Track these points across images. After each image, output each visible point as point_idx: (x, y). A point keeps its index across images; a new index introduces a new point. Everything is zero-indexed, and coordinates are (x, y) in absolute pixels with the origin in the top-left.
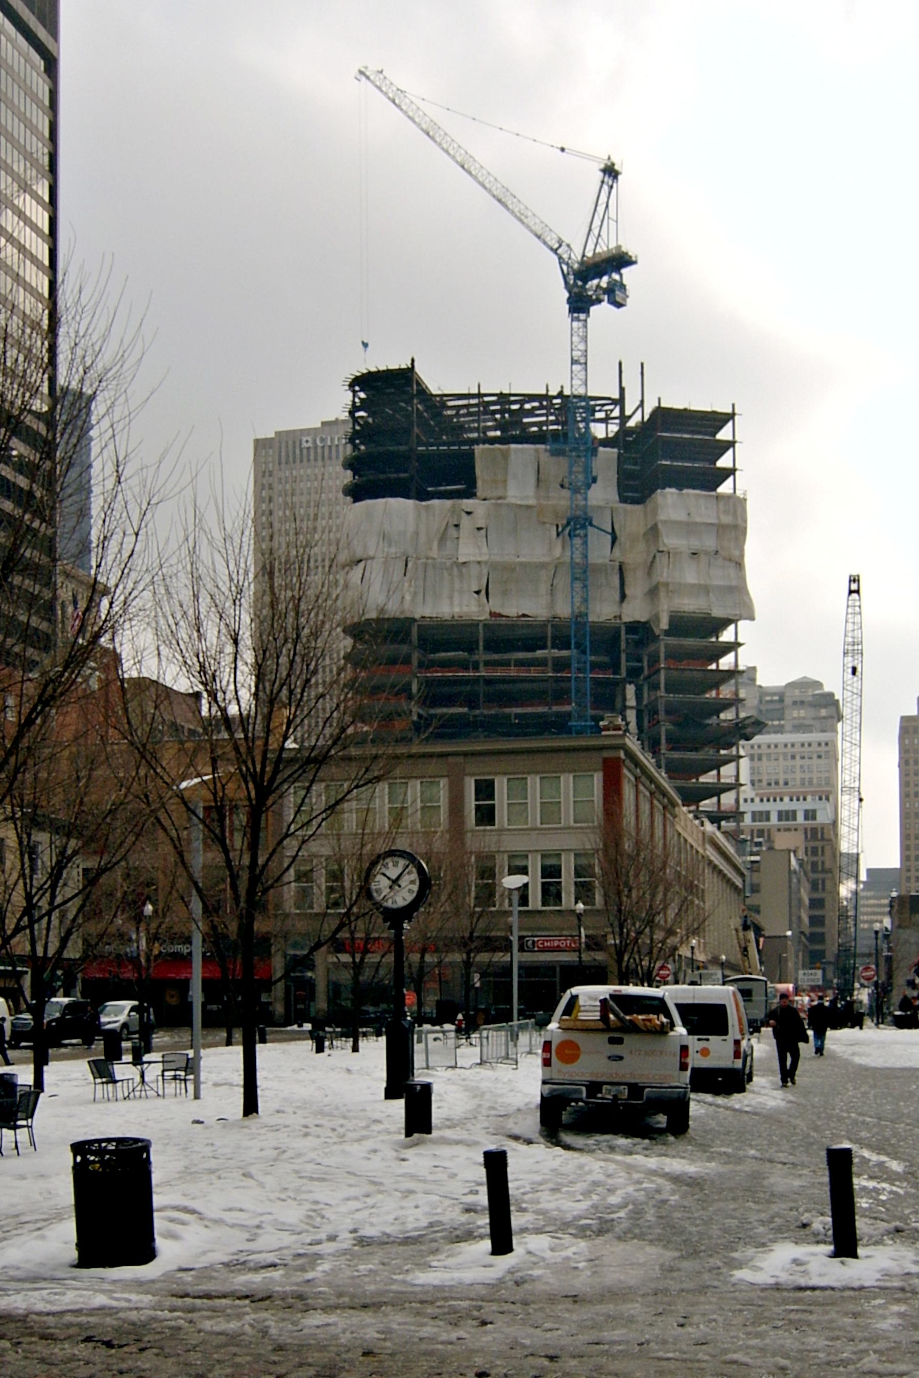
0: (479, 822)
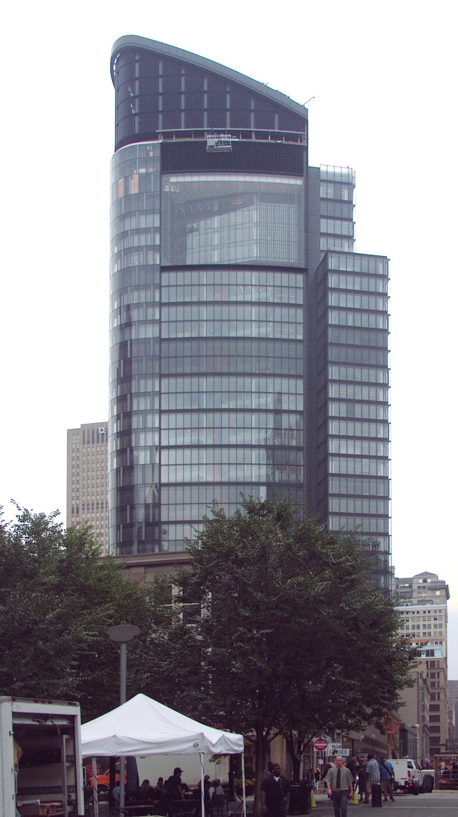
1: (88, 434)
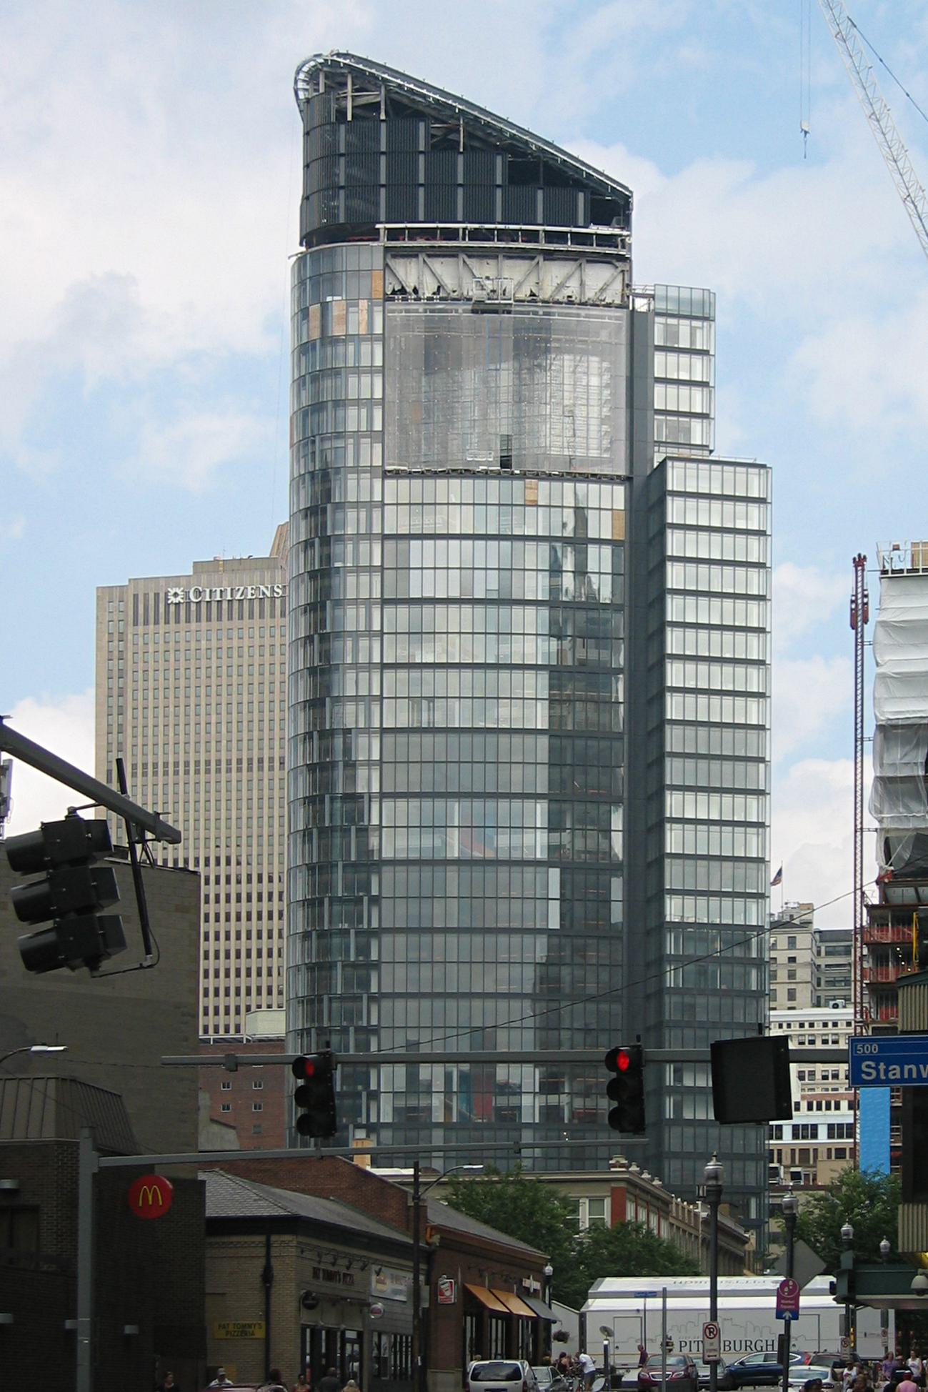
0: (792, 1173)
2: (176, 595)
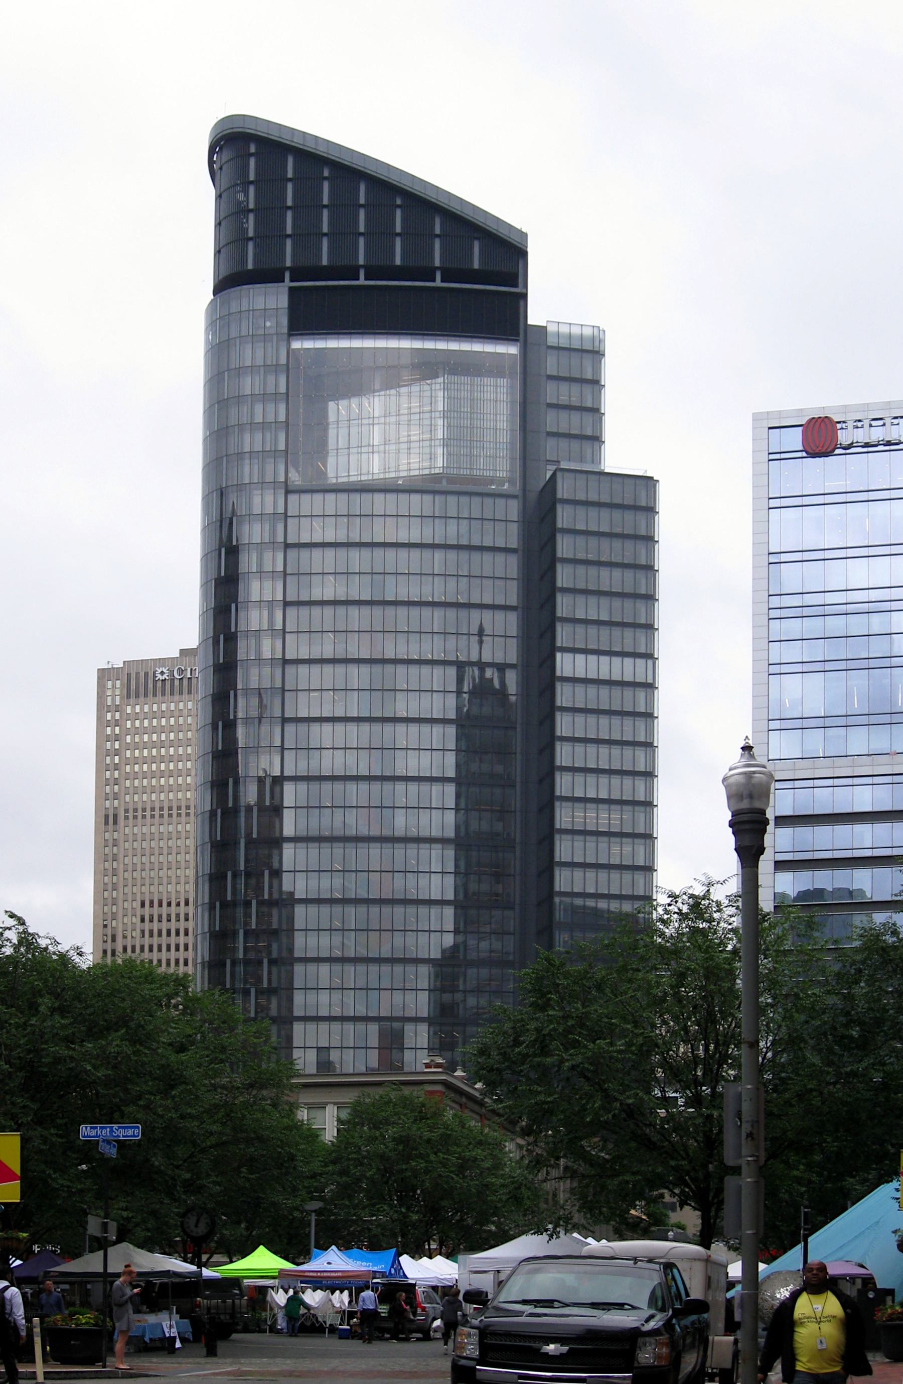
1: (137, 678)
2: (162, 674)
